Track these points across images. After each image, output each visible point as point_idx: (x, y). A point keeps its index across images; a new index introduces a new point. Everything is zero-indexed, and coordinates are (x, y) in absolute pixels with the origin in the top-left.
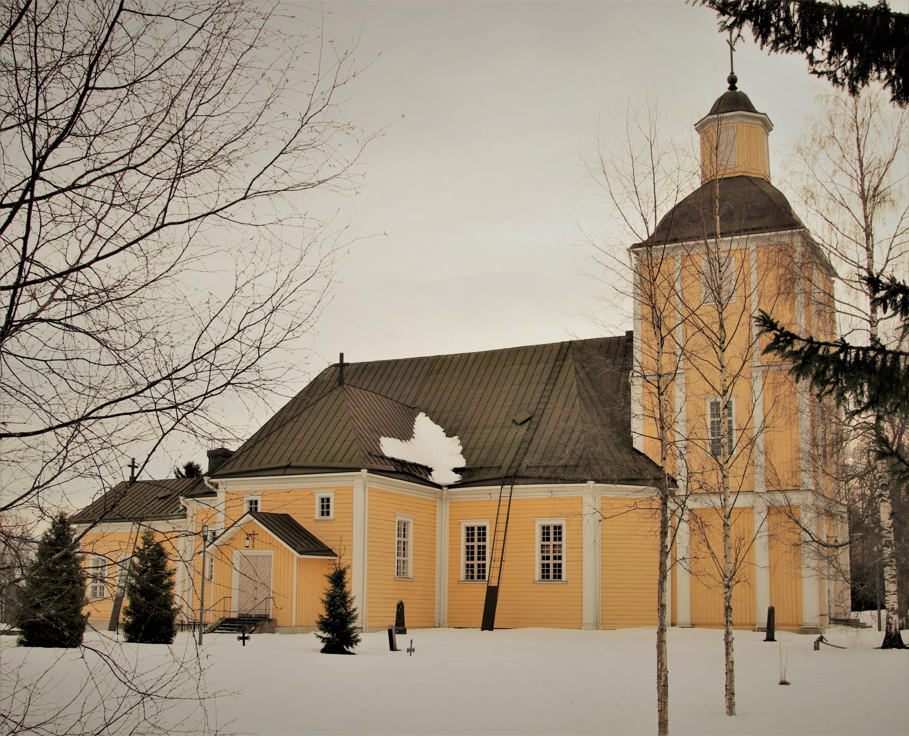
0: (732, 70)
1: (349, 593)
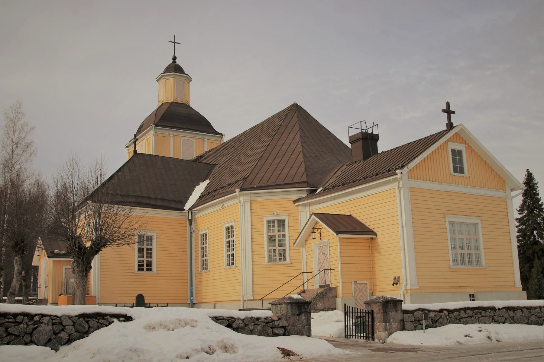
0: (174, 53)
1: (38, 184)
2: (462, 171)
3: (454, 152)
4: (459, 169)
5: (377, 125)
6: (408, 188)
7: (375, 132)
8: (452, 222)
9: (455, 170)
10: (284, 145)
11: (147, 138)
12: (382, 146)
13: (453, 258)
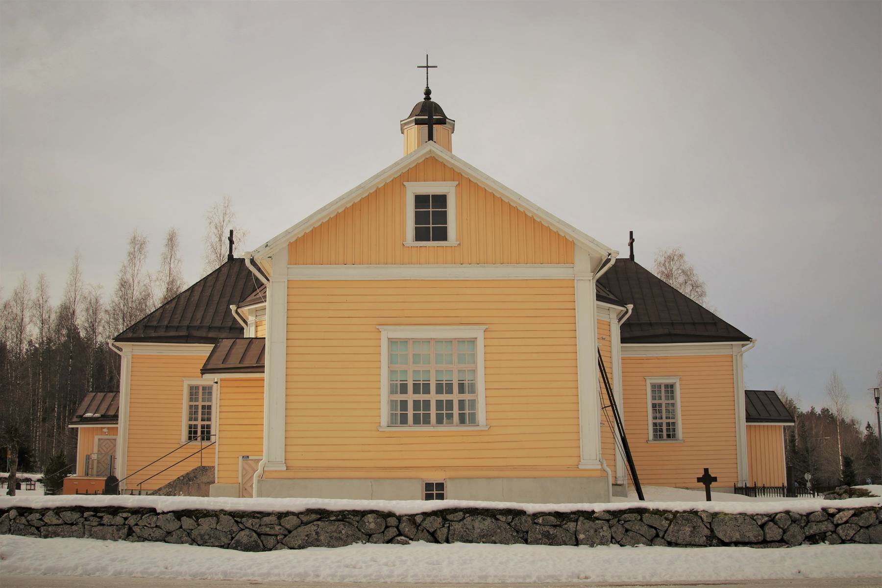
0: (427, 85)
6: (285, 282)
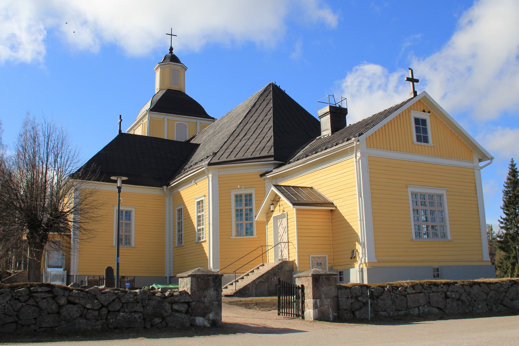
2: (426, 140)
3: (417, 121)
4: (422, 137)
5: (346, 99)
7: (344, 106)
8: (415, 193)
9: (419, 139)
10: (256, 122)
11: (144, 123)
12: (351, 120)
13: (415, 229)
